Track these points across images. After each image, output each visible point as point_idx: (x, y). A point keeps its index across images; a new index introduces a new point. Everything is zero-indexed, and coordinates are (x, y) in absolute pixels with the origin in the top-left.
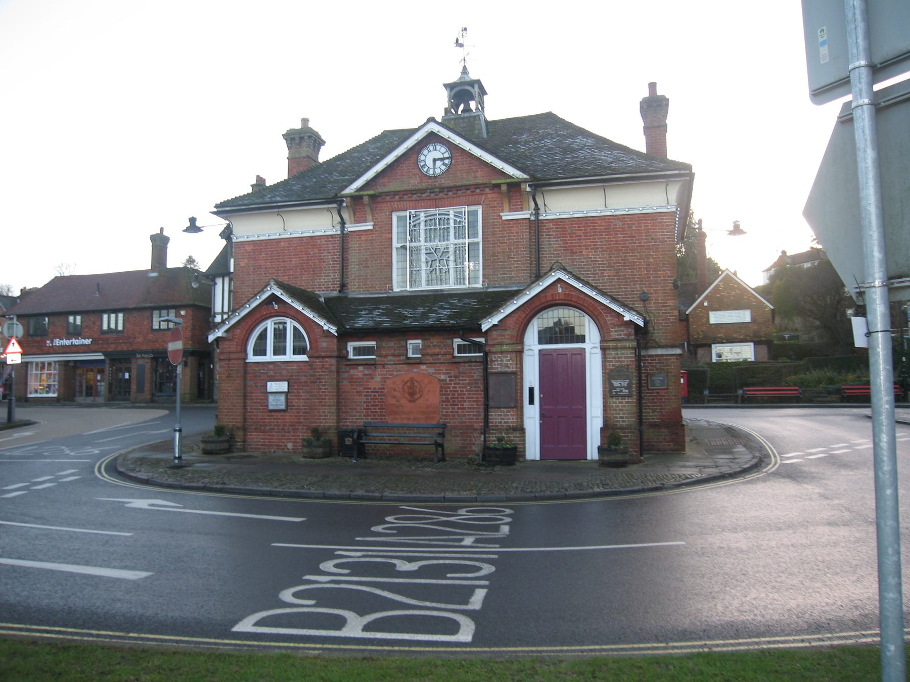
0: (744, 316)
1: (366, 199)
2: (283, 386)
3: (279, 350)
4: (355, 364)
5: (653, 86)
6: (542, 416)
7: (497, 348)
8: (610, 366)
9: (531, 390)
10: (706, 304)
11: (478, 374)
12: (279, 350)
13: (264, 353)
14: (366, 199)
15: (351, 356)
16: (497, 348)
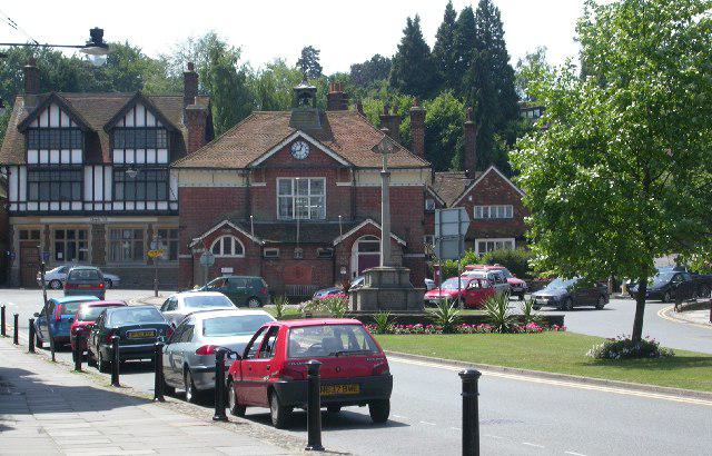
3: (227, 250)
12: (227, 250)
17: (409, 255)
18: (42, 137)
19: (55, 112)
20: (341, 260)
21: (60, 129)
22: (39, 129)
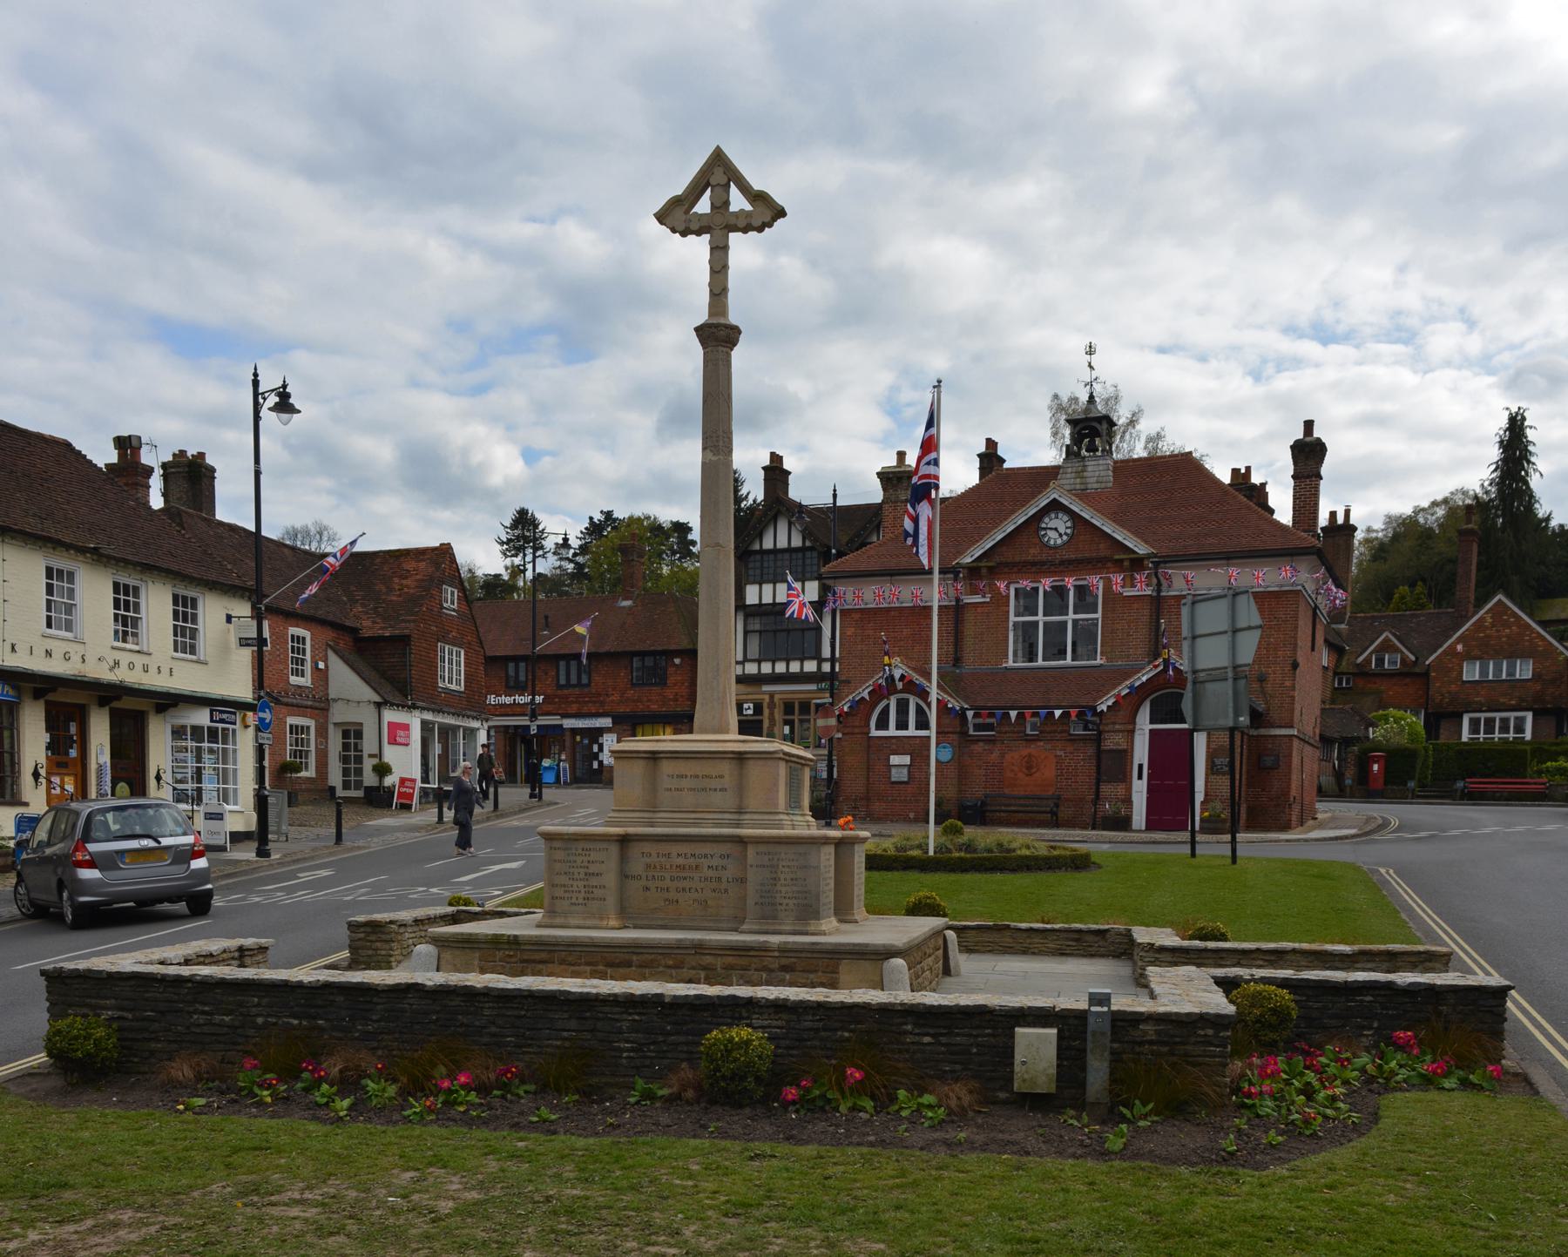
0: (1524, 670)
1: (984, 571)
2: (906, 760)
3: (902, 725)
4: (977, 740)
5: (1309, 425)
6: (1150, 790)
7: (1110, 727)
8: (1213, 746)
9: (1141, 766)
10: (1460, 647)
11: (1091, 750)
12: (902, 725)
13: (886, 727)
14: (984, 571)
15: (971, 732)
16: (1110, 727)
17: (1263, 731)
18: (808, 562)
19: (782, 527)
20: (1113, 741)
21: (790, 550)
22: (763, 552)
